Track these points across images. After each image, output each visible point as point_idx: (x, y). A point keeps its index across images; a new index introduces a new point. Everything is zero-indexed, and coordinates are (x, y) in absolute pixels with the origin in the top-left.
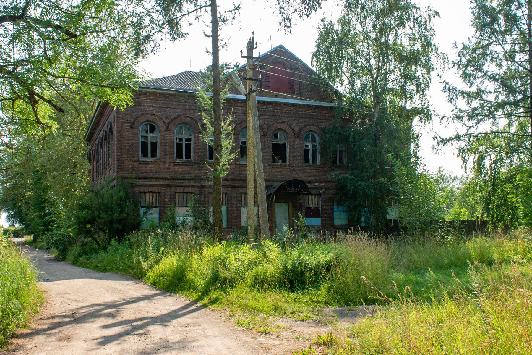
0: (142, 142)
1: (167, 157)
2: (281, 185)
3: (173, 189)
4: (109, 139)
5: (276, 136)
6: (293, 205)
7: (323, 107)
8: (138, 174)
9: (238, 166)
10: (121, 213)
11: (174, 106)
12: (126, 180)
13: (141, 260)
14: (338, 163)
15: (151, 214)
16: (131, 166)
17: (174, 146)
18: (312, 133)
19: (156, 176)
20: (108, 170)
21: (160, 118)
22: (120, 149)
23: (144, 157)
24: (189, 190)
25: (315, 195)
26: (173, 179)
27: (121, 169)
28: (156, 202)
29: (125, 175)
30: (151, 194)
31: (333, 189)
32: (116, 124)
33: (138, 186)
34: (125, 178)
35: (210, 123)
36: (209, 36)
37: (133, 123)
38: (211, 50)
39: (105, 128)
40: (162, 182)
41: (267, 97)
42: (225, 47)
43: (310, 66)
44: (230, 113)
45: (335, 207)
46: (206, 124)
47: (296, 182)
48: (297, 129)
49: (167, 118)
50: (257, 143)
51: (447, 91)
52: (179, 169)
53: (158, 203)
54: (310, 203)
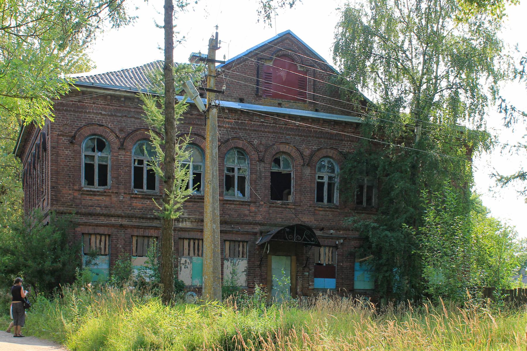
0: (86, 164)
1: (121, 186)
2: (279, 232)
3: (129, 231)
4: (43, 156)
5: (277, 161)
6: (298, 260)
7: (347, 123)
8: (81, 208)
10: (54, 261)
11: (132, 114)
12: (63, 216)
13: (64, 321)
14: (364, 204)
15: (95, 264)
16: (71, 197)
17: (130, 171)
18: (329, 159)
19: (105, 212)
20: (42, 200)
21: (112, 131)
22: (56, 173)
23: (88, 184)
24: (153, 233)
25: (330, 247)
26: (130, 217)
27: (57, 201)
28: (105, 248)
29: (62, 209)
30: (98, 237)
31: (355, 239)
32: (49, 136)
33: (79, 224)
34: (62, 213)
35: (160, 146)
36: (161, 27)
37: (74, 137)
38: (163, 46)
39: (38, 141)
40: (113, 220)
41: (266, 105)
42: (183, 42)
43: (330, 62)
44: (187, 134)
45: (357, 266)
46: (155, 148)
47: (301, 229)
48: (307, 152)
49: (121, 130)
50: (213, 176)
51: (503, 111)
52: (138, 204)
53: (107, 249)
54: (322, 257)
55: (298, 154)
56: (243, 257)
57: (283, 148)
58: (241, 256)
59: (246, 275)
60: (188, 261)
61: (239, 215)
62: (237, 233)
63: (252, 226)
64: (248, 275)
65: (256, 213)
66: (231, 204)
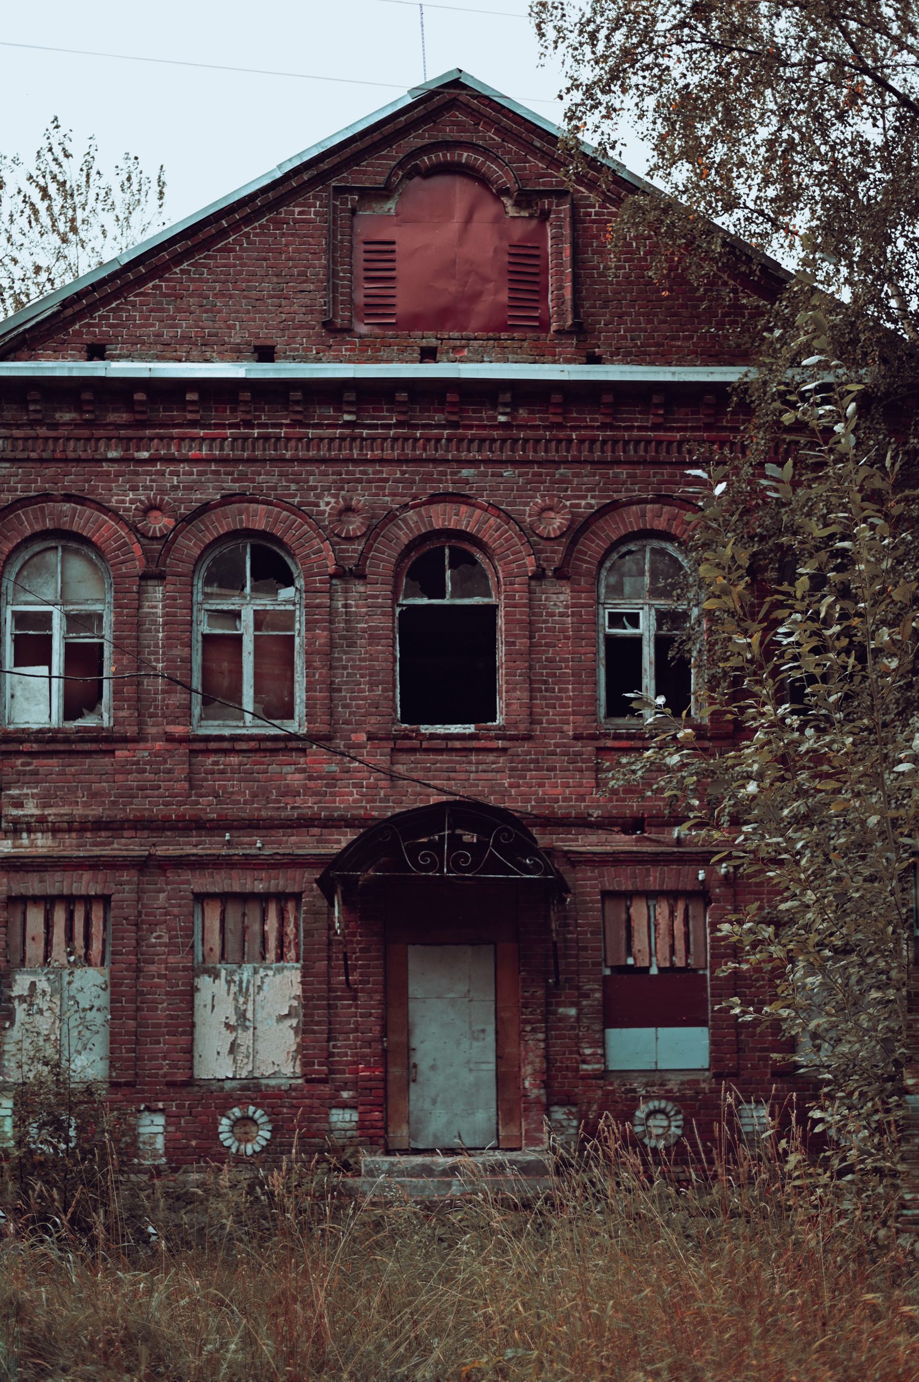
9: (183, 749)
18: (656, 544)
54: (640, 942)
55: (512, 531)
56: (280, 957)
57: (443, 517)
58: (271, 955)
59: (296, 1030)
60: (43, 984)
61: (260, 794)
62: (249, 863)
63: (315, 831)
64: (303, 1030)
65: (332, 780)
66: (226, 752)
